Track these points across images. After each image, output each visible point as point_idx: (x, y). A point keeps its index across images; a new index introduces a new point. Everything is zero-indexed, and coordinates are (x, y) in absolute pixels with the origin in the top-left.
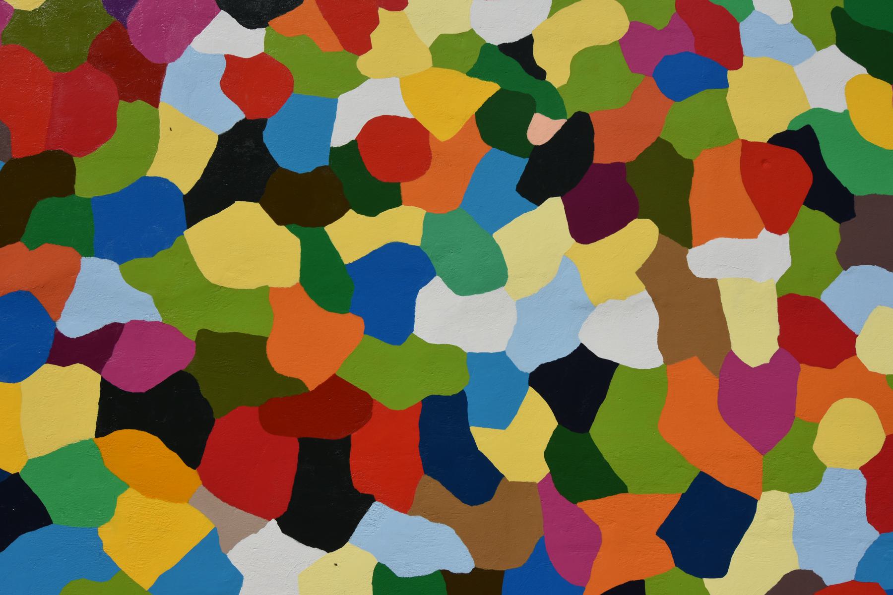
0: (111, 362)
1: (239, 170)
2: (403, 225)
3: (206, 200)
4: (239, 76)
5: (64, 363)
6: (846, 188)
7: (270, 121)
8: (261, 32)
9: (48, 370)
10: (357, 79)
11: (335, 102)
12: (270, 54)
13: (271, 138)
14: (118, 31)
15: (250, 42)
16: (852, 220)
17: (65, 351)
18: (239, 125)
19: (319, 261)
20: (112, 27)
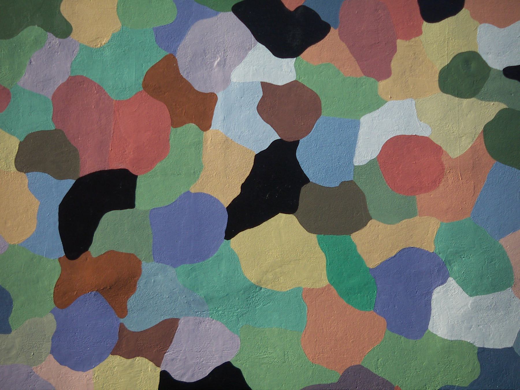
0: (168, 355)
1: (274, 185)
2: (425, 232)
3: (246, 212)
4: (273, 101)
5: (129, 355)
6: (243, 186)
7: (301, 141)
8: (289, 63)
9: (115, 361)
10: (376, 103)
11: (357, 125)
12: (300, 81)
13: (303, 155)
14: (169, 63)
15: (283, 71)
16: (236, 364)
17: (130, 345)
18: (275, 144)
19: (343, 267)
20: (166, 58)
